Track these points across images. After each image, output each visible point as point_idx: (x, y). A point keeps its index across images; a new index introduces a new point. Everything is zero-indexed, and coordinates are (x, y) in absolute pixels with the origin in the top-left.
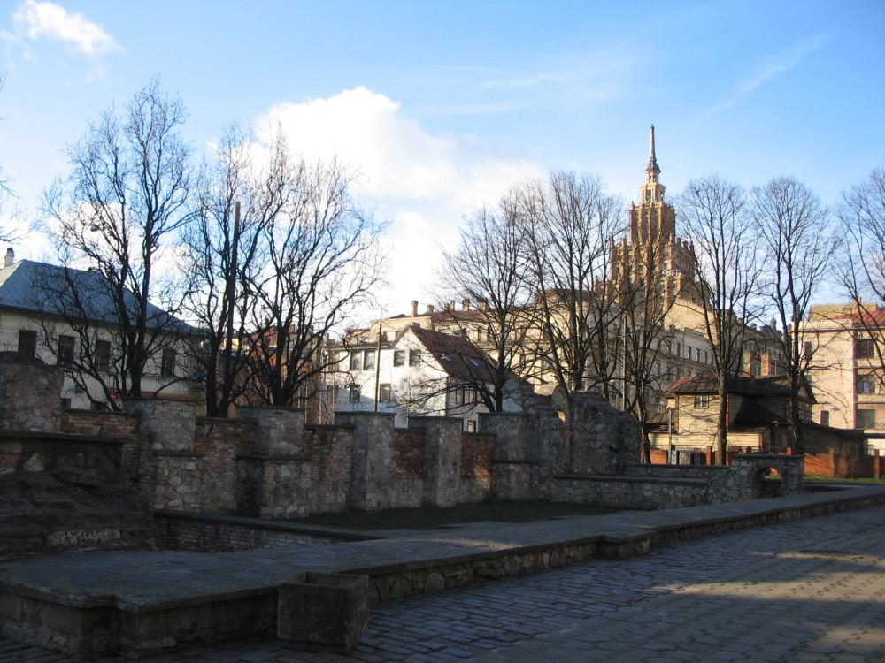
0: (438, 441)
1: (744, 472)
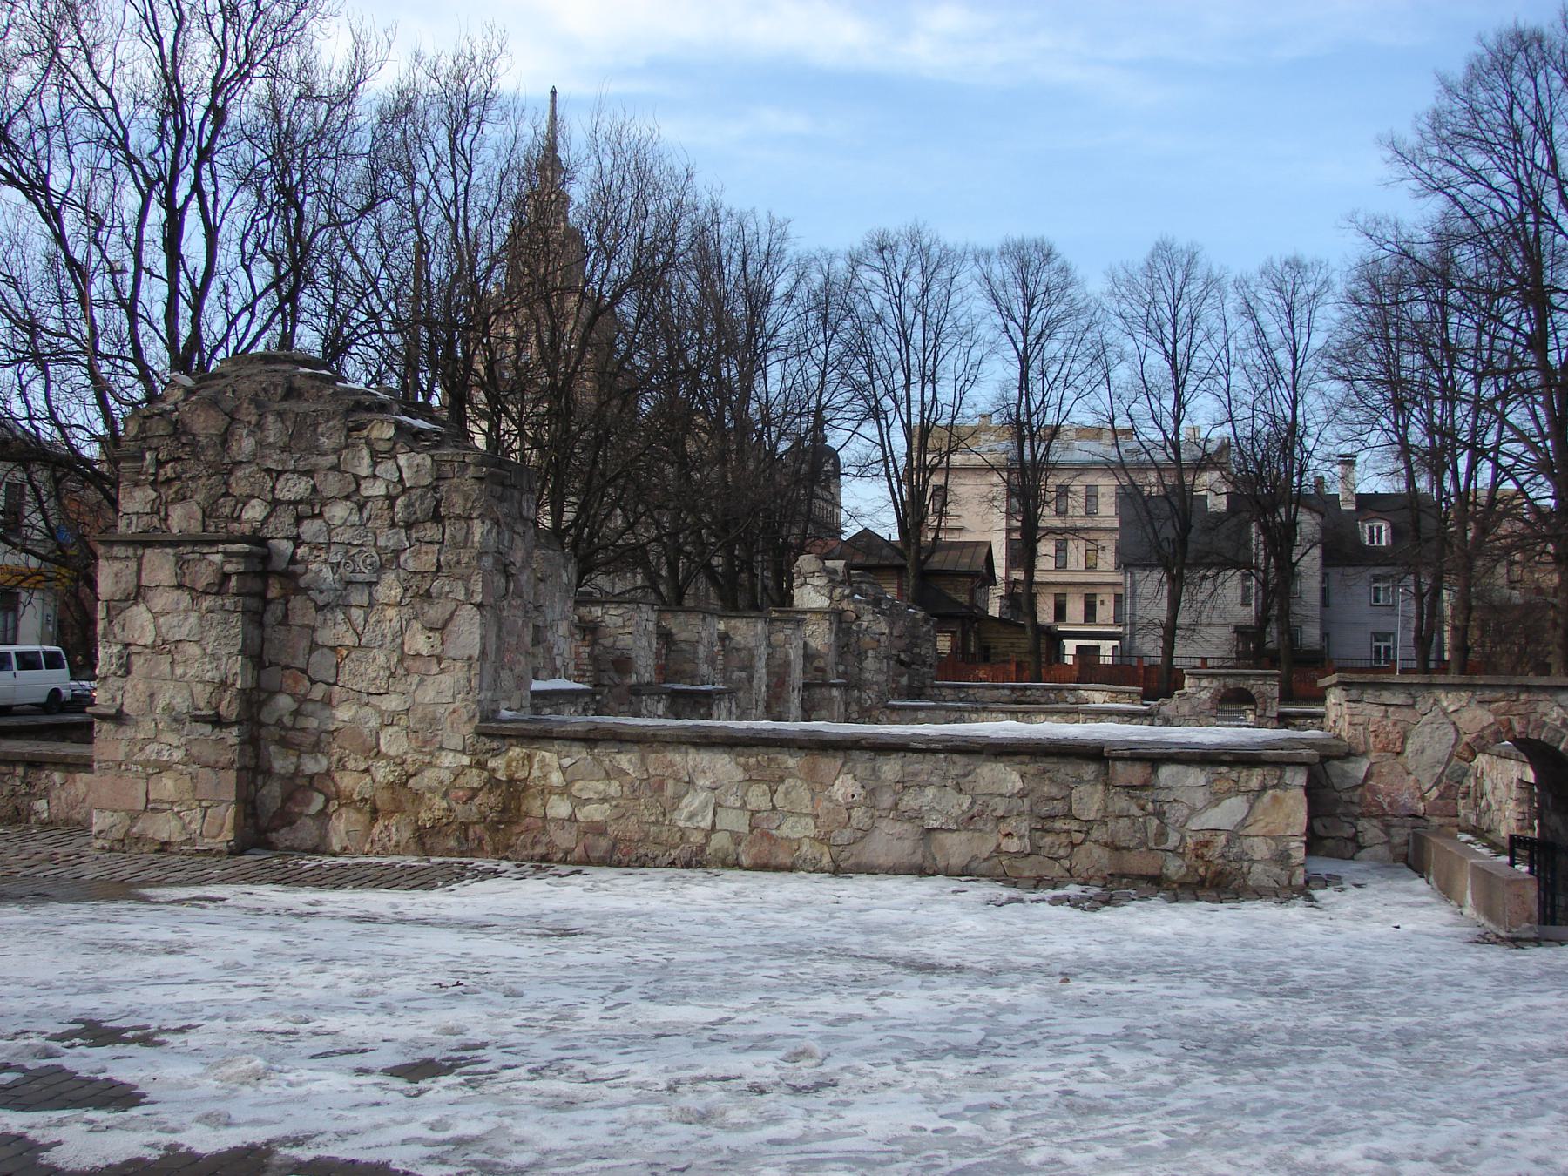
1: (1205, 695)
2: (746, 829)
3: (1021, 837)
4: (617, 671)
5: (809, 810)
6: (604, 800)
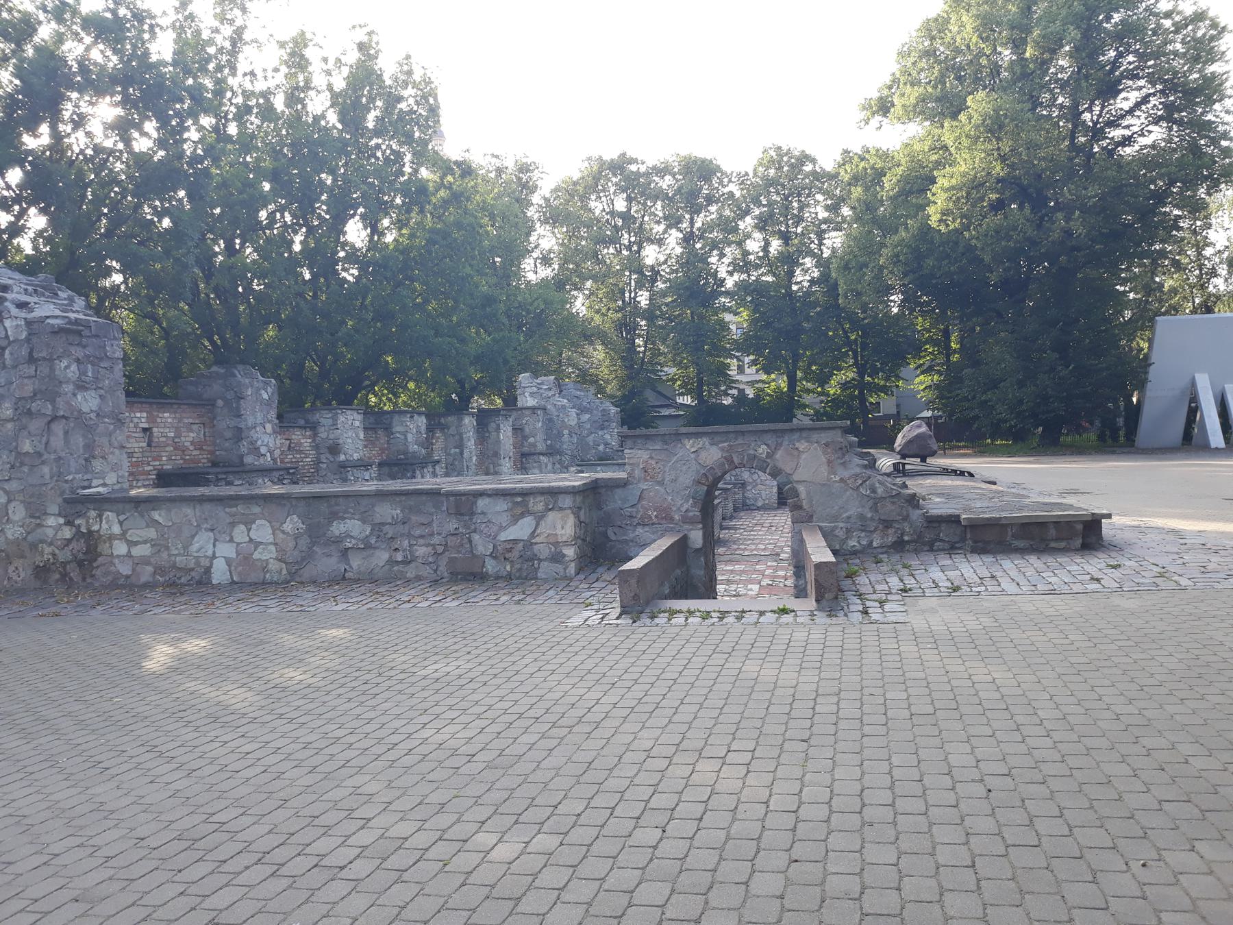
0: (498, 437)
2: (234, 555)
3: (404, 551)
4: (331, 453)
5: (271, 540)
6: (145, 542)
